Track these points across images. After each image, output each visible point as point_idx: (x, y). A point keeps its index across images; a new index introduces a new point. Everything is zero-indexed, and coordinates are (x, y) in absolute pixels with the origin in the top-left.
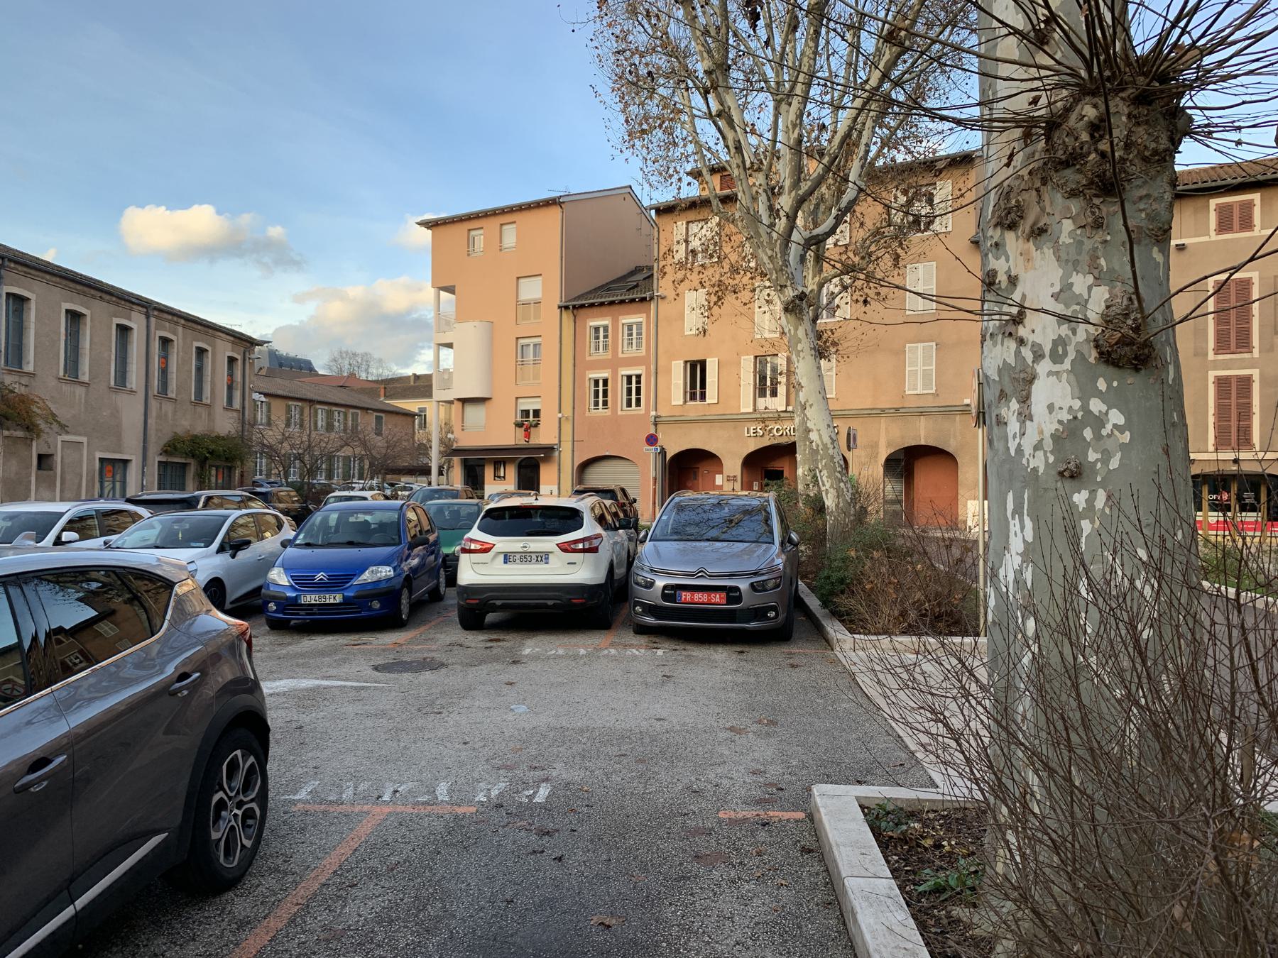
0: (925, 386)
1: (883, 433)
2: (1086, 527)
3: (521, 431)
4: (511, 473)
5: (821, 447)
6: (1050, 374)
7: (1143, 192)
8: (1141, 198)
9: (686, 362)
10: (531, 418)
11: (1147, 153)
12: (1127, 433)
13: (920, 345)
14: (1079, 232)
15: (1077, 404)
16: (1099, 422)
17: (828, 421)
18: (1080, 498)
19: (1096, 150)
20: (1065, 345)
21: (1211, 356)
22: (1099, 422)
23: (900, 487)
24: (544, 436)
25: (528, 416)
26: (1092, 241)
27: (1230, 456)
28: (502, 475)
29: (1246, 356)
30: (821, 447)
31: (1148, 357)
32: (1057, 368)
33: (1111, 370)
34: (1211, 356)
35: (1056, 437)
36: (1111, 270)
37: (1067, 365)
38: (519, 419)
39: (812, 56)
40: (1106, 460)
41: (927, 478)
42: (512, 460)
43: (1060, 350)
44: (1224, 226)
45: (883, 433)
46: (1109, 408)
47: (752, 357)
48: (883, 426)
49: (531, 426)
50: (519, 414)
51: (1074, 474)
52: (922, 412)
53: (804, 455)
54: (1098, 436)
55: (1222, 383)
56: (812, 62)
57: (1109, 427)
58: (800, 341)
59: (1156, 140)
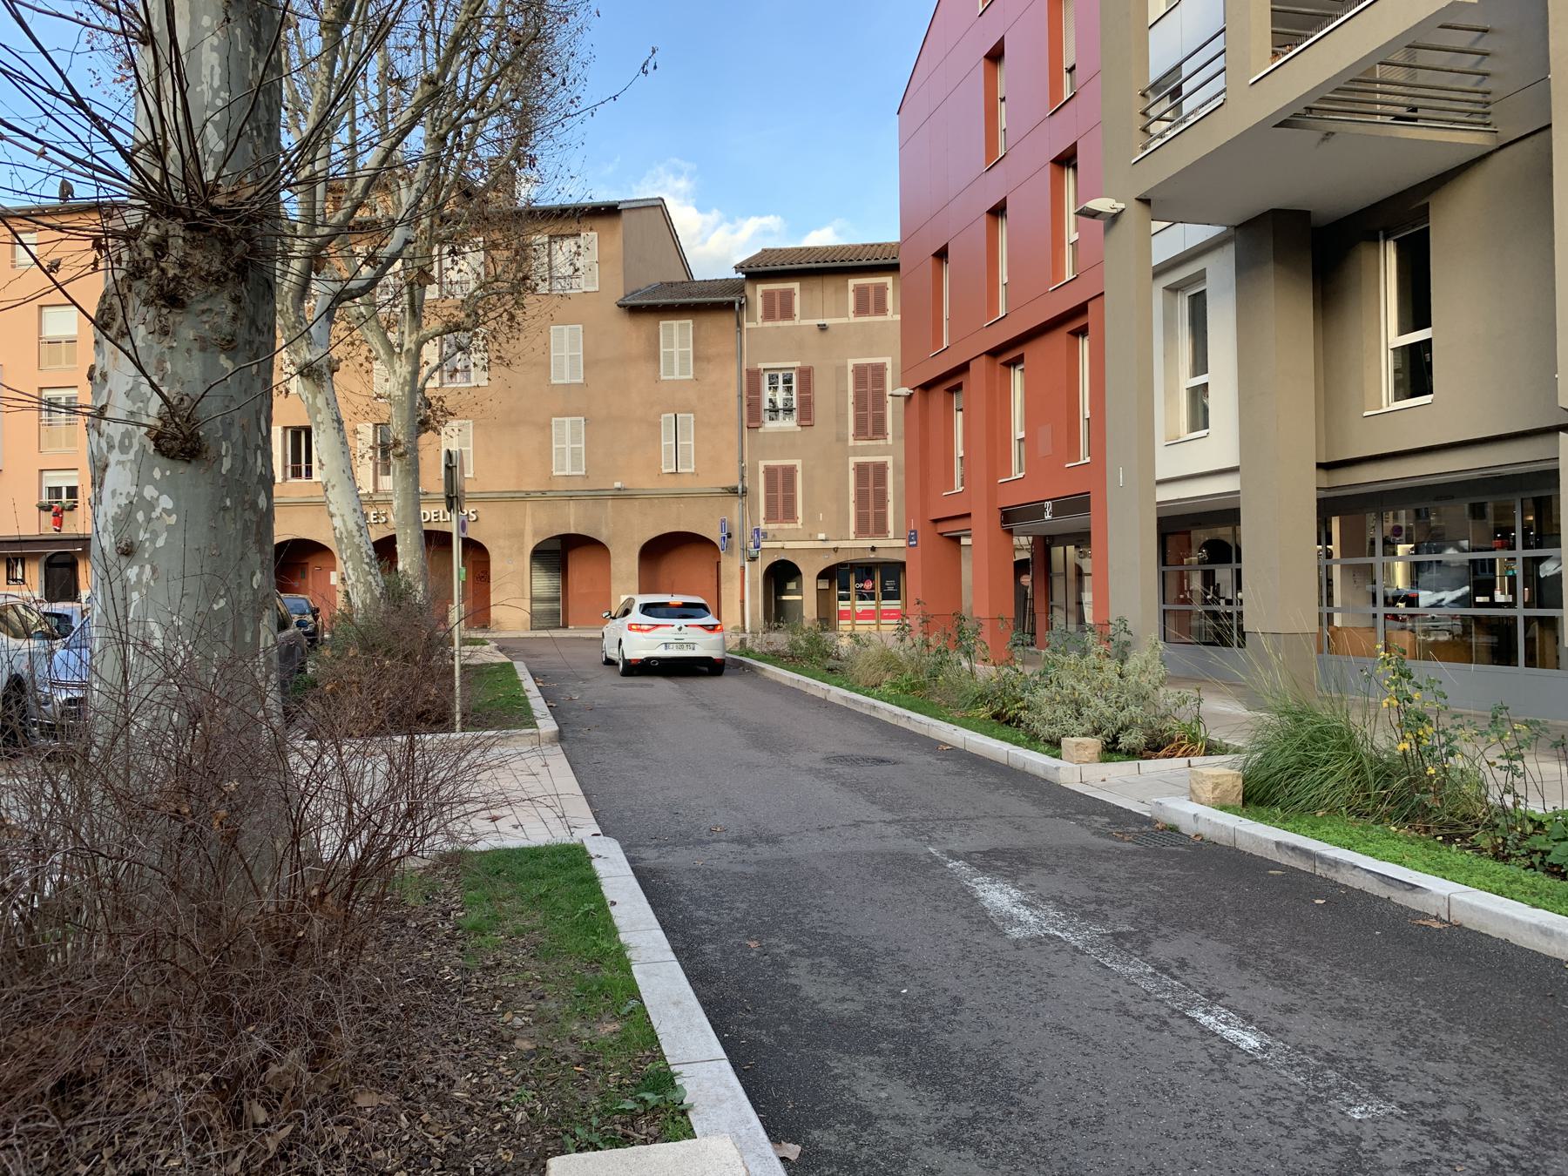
0: (574, 467)
1: (528, 520)
2: (135, 596)
3: (48, 517)
4: (34, 575)
5: (345, 534)
6: (119, 463)
7: (204, 306)
8: (203, 312)
9: (285, 428)
10: (64, 499)
11: (203, 274)
12: (174, 516)
13: (567, 420)
14: (150, 337)
15: (133, 490)
16: (151, 505)
17: (355, 504)
18: (132, 573)
19: (158, 266)
20: (130, 439)
21: (851, 442)
22: (151, 505)
23: (557, 582)
24: (78, 524)
25: (59, 495)
26: (160, 346)
27: (868, 543)
28: (19, 577)
29: (881, 442)
30: (345, 534)
31: (199, 451)
32: (124, 458)
33: (164, 461)
34: (851, 442)
35: (115, 520)
36: (174, 373)
37: (131, 456)
38: (45, 500)
39: (326, 83)
40: (153, 540)
41: (580, 567)
42: (35, 557)
43: (127, 441)
44: (861, 309)
45: (528, 520)
46: (161, 494)
47: (371, 425)
48: (529, 512)
49: (63, 509)
50: (45, 493)
51: (128, 551)
52: (571, 497)
53: (405, 544)
54: (149, 520)
55: (861, 469)
56: (325, 89)
57: (158, 510)
58: (319, 411)
59: (210, 263)
